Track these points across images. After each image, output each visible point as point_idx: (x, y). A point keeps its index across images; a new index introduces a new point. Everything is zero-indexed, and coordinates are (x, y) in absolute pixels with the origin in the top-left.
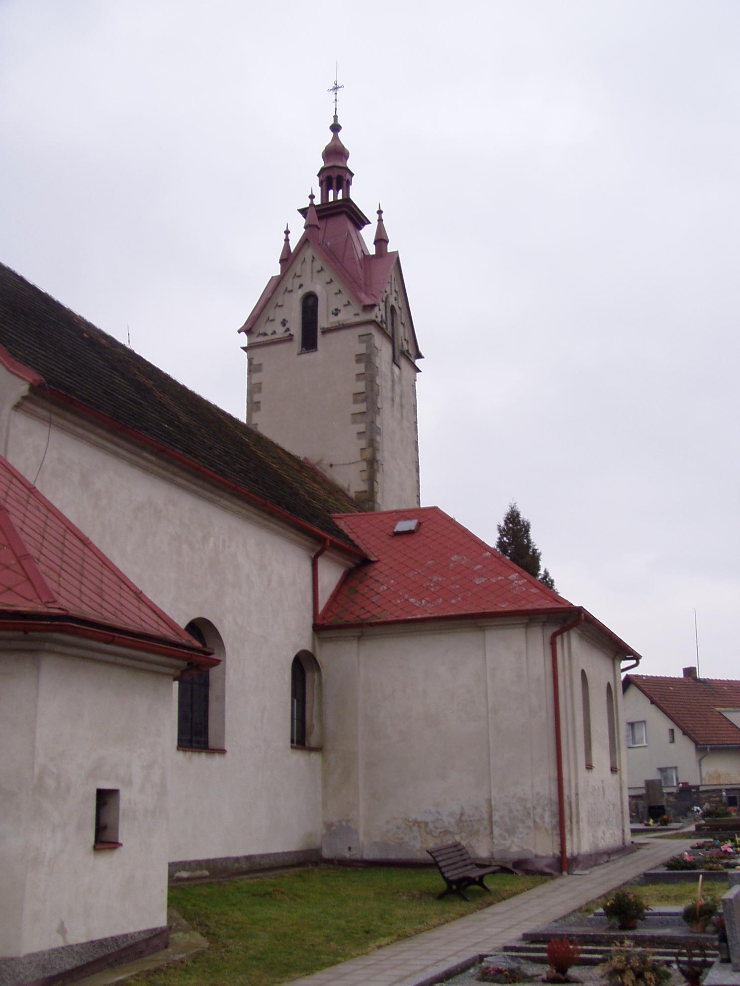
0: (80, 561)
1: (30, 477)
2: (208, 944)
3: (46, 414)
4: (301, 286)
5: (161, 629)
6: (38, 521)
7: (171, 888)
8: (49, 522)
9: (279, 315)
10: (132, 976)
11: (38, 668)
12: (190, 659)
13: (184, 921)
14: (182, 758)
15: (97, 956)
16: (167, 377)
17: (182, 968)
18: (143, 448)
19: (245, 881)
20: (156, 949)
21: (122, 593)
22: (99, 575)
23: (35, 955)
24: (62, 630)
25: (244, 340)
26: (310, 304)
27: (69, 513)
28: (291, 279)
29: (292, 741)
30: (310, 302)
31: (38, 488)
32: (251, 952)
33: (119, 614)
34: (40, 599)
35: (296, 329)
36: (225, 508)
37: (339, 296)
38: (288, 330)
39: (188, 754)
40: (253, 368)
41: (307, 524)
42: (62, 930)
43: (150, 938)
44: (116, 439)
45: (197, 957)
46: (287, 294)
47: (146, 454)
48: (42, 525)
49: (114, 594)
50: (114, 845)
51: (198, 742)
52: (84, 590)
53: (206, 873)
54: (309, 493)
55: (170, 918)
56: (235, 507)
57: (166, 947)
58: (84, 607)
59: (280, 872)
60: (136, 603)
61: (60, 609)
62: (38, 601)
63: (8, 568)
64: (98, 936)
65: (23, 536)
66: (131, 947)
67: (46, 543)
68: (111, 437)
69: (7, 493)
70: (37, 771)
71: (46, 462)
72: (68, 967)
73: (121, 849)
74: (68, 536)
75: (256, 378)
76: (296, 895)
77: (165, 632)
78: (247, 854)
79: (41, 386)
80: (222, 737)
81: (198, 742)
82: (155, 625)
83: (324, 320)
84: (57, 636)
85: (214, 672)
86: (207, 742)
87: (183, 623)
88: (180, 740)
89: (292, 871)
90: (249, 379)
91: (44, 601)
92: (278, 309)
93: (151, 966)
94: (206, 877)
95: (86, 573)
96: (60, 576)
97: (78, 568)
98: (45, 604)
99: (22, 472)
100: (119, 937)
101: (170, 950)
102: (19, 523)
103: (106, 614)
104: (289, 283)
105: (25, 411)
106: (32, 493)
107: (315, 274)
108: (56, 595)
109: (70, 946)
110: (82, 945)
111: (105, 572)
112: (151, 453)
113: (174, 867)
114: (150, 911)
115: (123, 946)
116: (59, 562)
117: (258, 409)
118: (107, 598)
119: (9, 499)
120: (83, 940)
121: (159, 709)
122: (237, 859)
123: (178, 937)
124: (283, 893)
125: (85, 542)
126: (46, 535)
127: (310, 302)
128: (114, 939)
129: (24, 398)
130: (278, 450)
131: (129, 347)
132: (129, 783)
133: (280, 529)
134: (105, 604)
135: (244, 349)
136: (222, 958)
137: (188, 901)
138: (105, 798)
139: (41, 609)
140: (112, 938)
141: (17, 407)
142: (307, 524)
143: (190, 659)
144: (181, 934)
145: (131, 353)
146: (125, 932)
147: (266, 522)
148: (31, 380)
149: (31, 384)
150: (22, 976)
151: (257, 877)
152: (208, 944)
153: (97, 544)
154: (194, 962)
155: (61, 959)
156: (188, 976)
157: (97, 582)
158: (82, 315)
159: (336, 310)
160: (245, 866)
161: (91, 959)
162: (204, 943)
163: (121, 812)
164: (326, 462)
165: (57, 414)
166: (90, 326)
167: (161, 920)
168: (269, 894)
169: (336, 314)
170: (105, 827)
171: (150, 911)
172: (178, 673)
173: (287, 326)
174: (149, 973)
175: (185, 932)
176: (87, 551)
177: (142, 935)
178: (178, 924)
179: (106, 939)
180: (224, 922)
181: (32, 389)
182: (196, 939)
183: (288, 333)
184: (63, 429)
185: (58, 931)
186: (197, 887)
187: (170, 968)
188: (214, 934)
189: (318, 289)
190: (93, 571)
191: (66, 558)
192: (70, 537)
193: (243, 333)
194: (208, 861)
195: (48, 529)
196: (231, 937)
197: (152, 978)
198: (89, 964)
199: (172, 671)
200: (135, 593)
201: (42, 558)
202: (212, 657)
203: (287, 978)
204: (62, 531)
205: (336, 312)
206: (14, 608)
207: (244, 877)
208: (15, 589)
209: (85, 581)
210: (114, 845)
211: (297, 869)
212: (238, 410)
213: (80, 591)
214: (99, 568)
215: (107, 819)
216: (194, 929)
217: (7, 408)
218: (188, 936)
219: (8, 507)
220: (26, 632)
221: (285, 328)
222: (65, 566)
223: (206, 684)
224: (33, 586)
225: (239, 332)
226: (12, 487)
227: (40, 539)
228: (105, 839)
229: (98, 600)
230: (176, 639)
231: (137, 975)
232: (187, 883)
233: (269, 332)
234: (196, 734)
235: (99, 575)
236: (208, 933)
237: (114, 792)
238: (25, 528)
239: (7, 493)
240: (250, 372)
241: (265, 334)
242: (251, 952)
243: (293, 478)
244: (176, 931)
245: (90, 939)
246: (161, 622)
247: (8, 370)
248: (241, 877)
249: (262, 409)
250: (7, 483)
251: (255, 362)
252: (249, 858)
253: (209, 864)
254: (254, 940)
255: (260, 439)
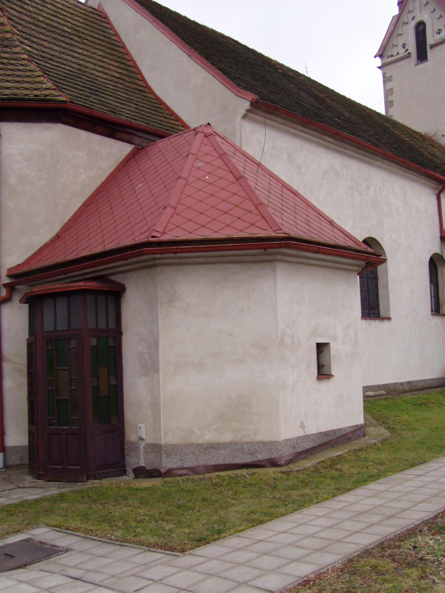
0: (293, 205)
1: (258, 158)
2: (389, 434)
3: (262, 119)
4: (414, 18)
5: (347, 242)
6: (265, 183)
7: (364, 401)
8: (271, 183)
9: (400, 41)
10: (345, 453)
11: (274, 271)
12: (367, 261)
13: (374, 421)
14: (365, 323)
15: (324, 441)
16: (333, 92)
17: (375, 448)
18: (325, 134)
19: (408, 397)
20: (359, 437)
21: (322, 223)
22: (306, 213)
23: (288, 440)
24: (286, 246)
25: (378, 62)
26: (420, 30)
27: (284, 178)
28: (406, 15)
29: (432, 311)
30: (421, 28)
31: (263, 163)
32: (417, 439)
33: (321, 235)
34: (271, 228)
35: (412, 48)
36: (379, 167)
37: (440, 20)
38: (407, 50)
39: (368, 321)
40: (386, 80)
41: (433, 173)
42: (302, 426)
43: (354, 431)
44: (306, 130)
45: (384, 441)
46: (404, 25)
47: (326, 138)
48: (268, 185)
49: (315, 222)
50: (329, 376)
51: (374, 314)
52: (298, 221)
53: (384, 392)
54: (430, 154)
55: (365, 419)
56: (384, 166)
57: (364, 436)
58: (299, 232)
59: (428, 391)
60: (330, 227)
61: (284, 233)
62: (270, 230)
63: (250, 212)
64: (324, 429)
65: (257, 192)
66: (345, 435)
67: (271, 196)
68: (302, 128)
69: (244, 168)
70: (279, 333)
71: (266, 149)
72: (308, 447)
73: (331, 381)
74: (284, 191)
75: (389, 85)
76: (441, 405)
77: (351, 245)
78: (408, 381)
79: (257, 102)
80: (388, 308)
81: (374, 314)
82: (344, 240)
83: (431, 39)
84: (283, 250)
85: (380, 268)
86: (379, 314)
87: (361, 239)
88: (362, 313)
89: (436, 390)
90: (385, 87)
91: (274, 229)
92: (399, 37)
93: (356, 447)
94: (384, 395)
95: (297, 212)
96: (282, 214)
97: (292, 209)
98: (275, 231)
99: (252, 155)
100: (336, 430)
101: (367, 437)
102: (255, 185)
103: (313, 235)
104: (405, 19)
105: (248, 118)
106: (260, 167)
107: (423, 8)
108: (281, 226)
109: (308, 435)
110: (314, 435)
111: (309, 210)
112: (329, 137)
113: (366, 389)
114: (353, 415)
115: (339, 435)
116: (281, 206)
117: (392, 106)
118: (312, 225)
119: (246, 172)
120: (315, 432)
121: (348, 292)
122: (402, 384)
123: (369, 429)
124: (433, 403)
125: (295, 193)
126: (271, 191)
127: (421, 28)
128: (334, 431)
129: (248, 111)
130: (408, 130)
131: (307, 75)
132: (335, 339)
133: (414, 177)
134: (311, 229)
135: (379, 68)
136: (399, 442)
137: (375, 409)
138: (321, 348)
139: (273, 234)
140: (332, 431)
141: (244, 117)
142: (433, 173)
143: (367, 261)
144: (372, 428)
145: (309, 79)
146: (339, 427)
147: (406, 174)
148: (251, 99)
149: (251, 102)
150: (282, 452)
151: (415, 394)
152: (389, 434)
153: (301, 193)
154: (382, 445)
155: (303, 442)
156: (379, 453)
157: (306, 217)
158: (276, 60)
159: (439, 30)
160: (407, 388)
161: (320, 443)
162: (387, 434)
163: (332, 357)
164: (440, 134)
165: (269, 119)
166: (282, 66)
167: (360, 421)
168: (424, 404)
169: (439, 33)
170: (323, 366)
171: (353, 415)
172: (360, 269)
173: (406, 48)
174: (355, 451)
175: (375, 427)
176: (296, 198)
177: (350, 429)
178: (370, 423)
179: (328, 431)
180: (398, 421)
181: (252, 104)
182: (381, 431)
183: (407, 53)
184: (273, 127)
185: (300, 427)
186: (380, 400)
187: (368, 448)
188: (393, 428)
189: (425, 17)
190: (301, 209)
191: (284, 204)
192: (285, 191)
193: (378, 58)
194: (384, 385)
195: (272, 187)
196: (403, 430)
197: (358, 454)
198: (320, 445)
199: (356, 268)
200: (330, 222)
201: (270, 205)
202: (381, 257)
203: (441, 454)
204: (281, 188)
205: (439, 32)
206: (256, 236)
207: (407, 394)
208: (256, 224)
209: (298, 216)
210: (329, 376)
211: (439, 389)
212: (379, 107)
213: (296, 222)
214: (305, 208)
215: (324, 361)
216: (380, 425)
217: (239, 119)
218: (376, 429)
219: (246, 175)
220: (265, 250)
221: (405, 50)
222: (284, 208)
223: (376, 278)
224: (265, 220)
225: (375, 57)
226: (247, 164)
227: (267, 193)
228: (323, 373)
229: (307, 227)
230: (357, 247)
231: (348, 452)
232: (373, 398)
233: (395, 54)
234: (372, 308)
235: (306, 213)
236: (389, 427)
237: (327, 344)
238: (258, 187)
239: (244, 168)
240: (385, 82)
241: (392, 56)
242: (417, 439)
243: (419, 145)
244: (369, 427)
245: (319, 431)
246: (347, 238)
247: (236, 95)
248: (405, 394)
249: (395, 106)
250: (244, 162)
251: (387, 75)
252: (409, 383)
253: (385, 387)
254: (418, 432)
255: (395, 124)
